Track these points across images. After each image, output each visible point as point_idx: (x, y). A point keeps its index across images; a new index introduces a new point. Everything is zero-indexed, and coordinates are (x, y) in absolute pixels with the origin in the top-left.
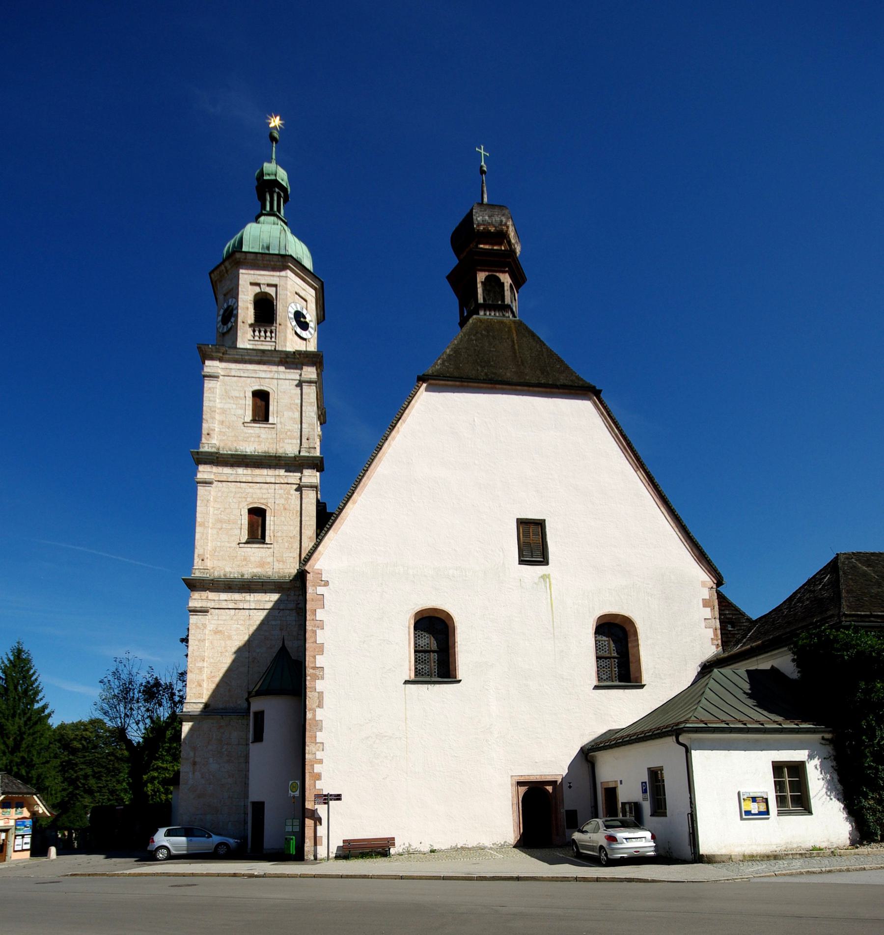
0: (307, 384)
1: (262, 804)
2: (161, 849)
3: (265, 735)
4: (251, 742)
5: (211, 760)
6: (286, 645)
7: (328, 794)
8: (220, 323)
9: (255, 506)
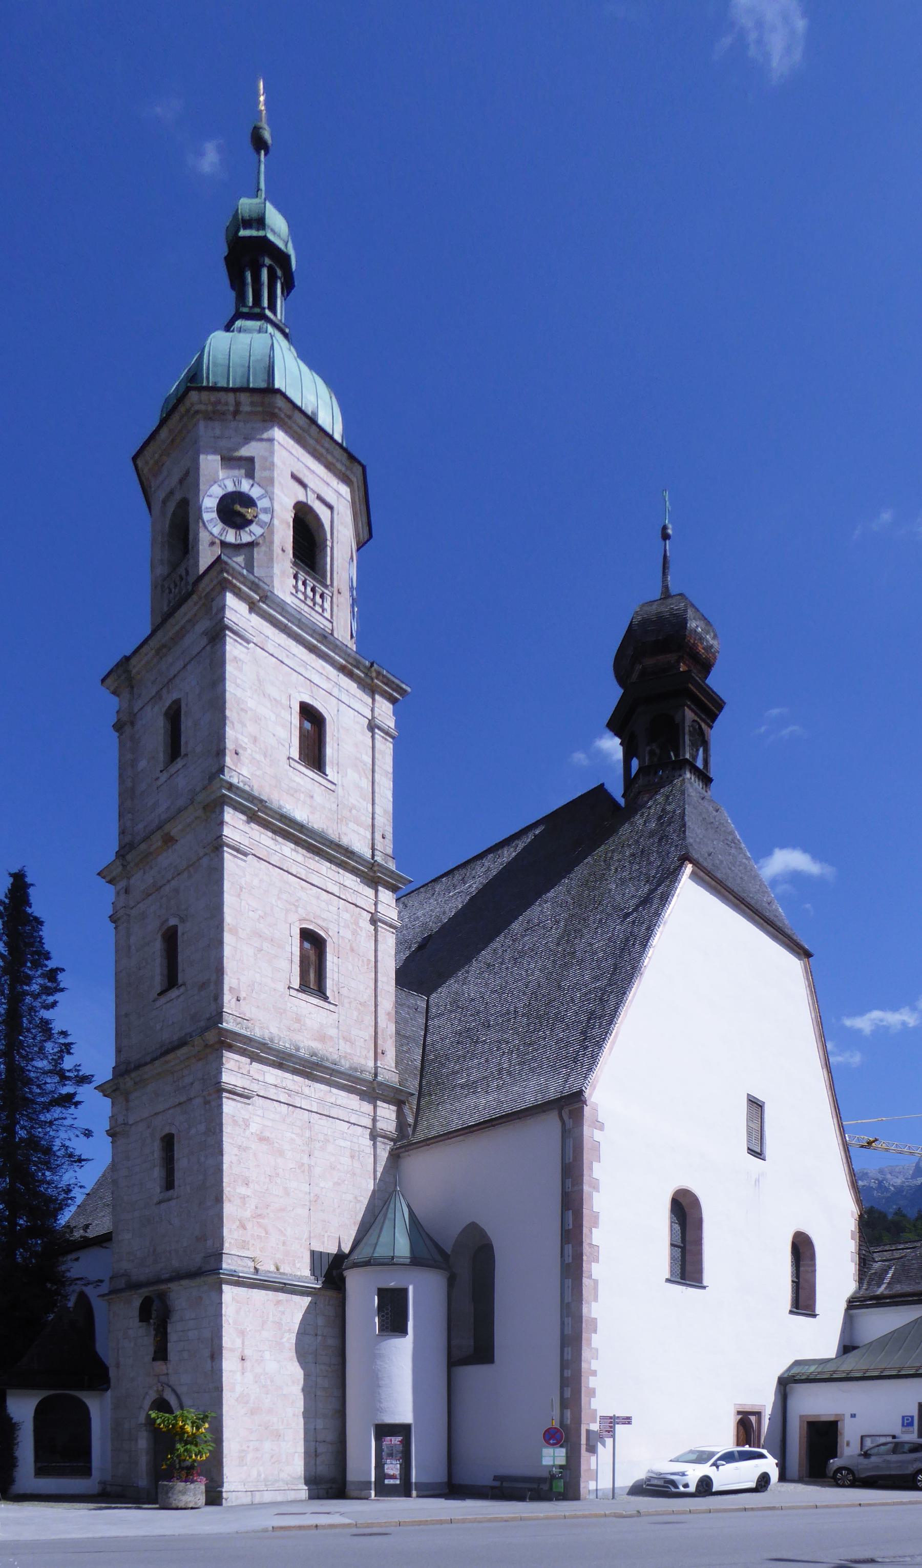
0: (382, 734)
5: (267, 1355)
7: (614, 1415)
9: (311, 927)
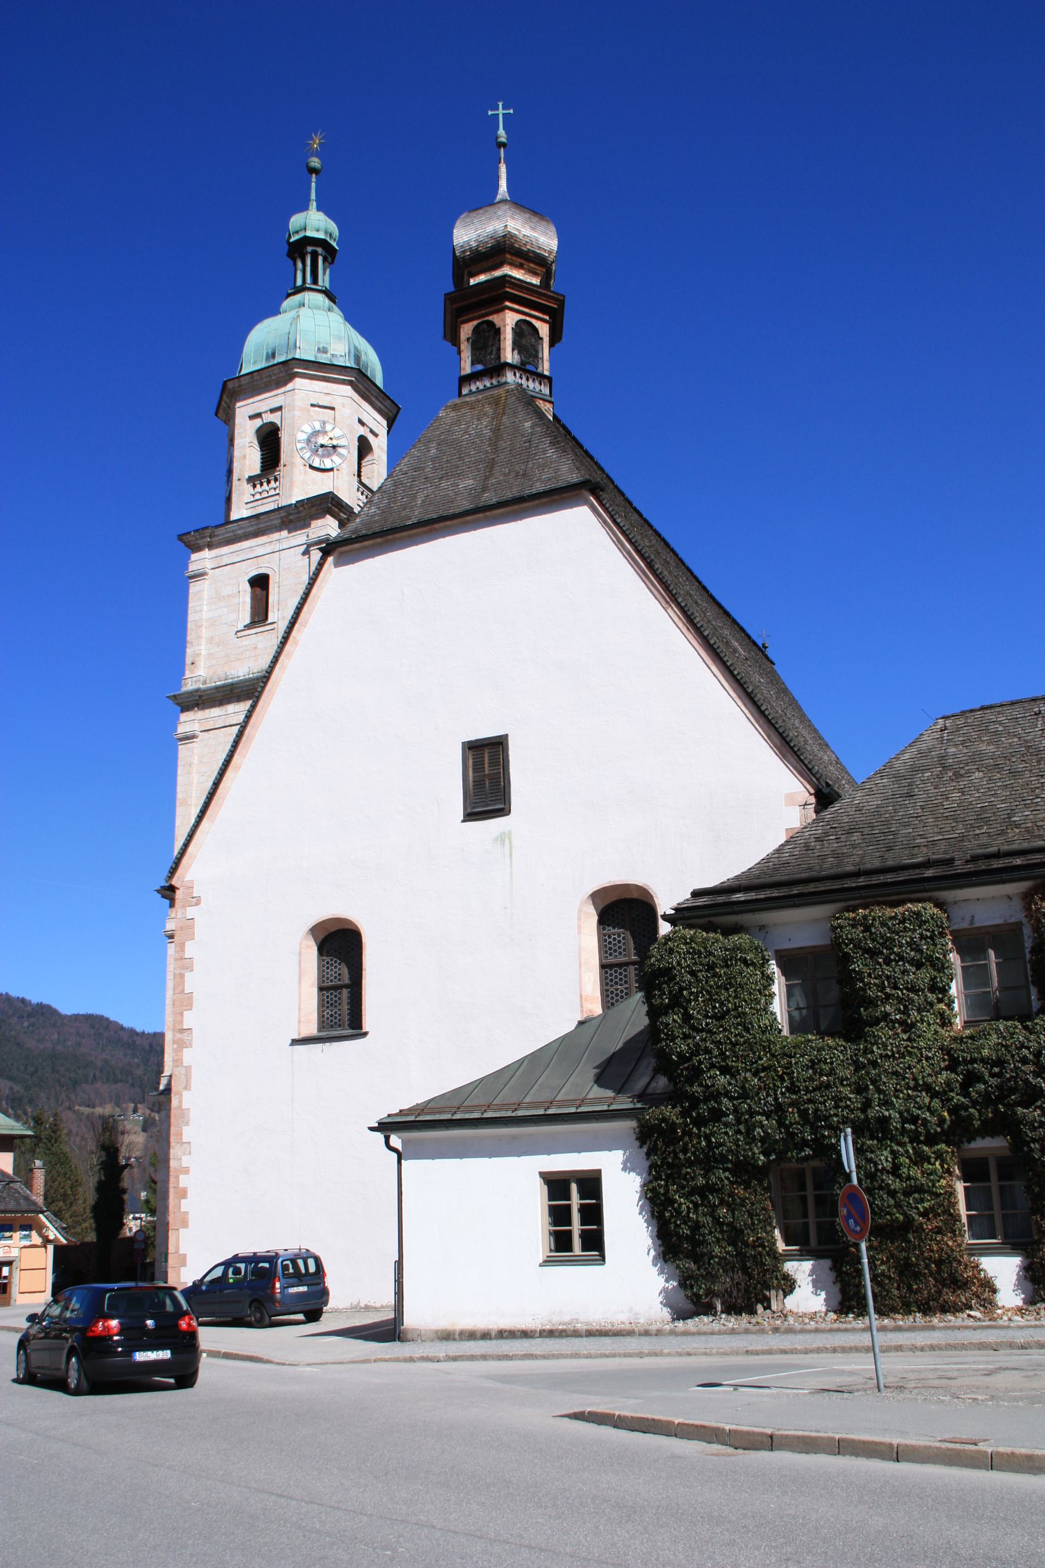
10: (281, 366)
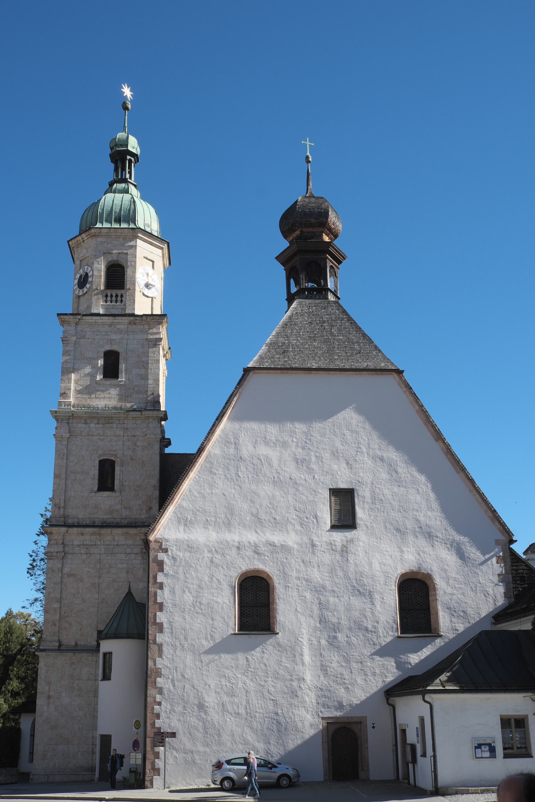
1: (110, 736)
2: (287, 777)
3: (113, 675)
4: (100, 679)
5: (64, 694)
6: (132, 591)
8: (77, 286)
9: (106, 458)
10: (130, 230)
